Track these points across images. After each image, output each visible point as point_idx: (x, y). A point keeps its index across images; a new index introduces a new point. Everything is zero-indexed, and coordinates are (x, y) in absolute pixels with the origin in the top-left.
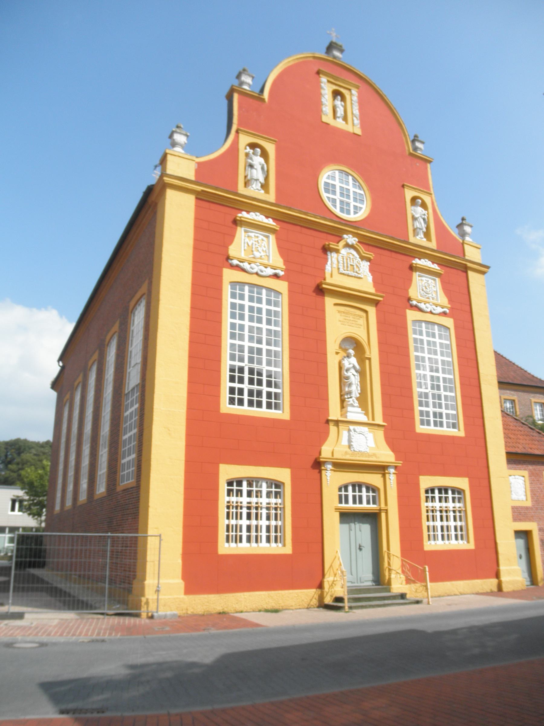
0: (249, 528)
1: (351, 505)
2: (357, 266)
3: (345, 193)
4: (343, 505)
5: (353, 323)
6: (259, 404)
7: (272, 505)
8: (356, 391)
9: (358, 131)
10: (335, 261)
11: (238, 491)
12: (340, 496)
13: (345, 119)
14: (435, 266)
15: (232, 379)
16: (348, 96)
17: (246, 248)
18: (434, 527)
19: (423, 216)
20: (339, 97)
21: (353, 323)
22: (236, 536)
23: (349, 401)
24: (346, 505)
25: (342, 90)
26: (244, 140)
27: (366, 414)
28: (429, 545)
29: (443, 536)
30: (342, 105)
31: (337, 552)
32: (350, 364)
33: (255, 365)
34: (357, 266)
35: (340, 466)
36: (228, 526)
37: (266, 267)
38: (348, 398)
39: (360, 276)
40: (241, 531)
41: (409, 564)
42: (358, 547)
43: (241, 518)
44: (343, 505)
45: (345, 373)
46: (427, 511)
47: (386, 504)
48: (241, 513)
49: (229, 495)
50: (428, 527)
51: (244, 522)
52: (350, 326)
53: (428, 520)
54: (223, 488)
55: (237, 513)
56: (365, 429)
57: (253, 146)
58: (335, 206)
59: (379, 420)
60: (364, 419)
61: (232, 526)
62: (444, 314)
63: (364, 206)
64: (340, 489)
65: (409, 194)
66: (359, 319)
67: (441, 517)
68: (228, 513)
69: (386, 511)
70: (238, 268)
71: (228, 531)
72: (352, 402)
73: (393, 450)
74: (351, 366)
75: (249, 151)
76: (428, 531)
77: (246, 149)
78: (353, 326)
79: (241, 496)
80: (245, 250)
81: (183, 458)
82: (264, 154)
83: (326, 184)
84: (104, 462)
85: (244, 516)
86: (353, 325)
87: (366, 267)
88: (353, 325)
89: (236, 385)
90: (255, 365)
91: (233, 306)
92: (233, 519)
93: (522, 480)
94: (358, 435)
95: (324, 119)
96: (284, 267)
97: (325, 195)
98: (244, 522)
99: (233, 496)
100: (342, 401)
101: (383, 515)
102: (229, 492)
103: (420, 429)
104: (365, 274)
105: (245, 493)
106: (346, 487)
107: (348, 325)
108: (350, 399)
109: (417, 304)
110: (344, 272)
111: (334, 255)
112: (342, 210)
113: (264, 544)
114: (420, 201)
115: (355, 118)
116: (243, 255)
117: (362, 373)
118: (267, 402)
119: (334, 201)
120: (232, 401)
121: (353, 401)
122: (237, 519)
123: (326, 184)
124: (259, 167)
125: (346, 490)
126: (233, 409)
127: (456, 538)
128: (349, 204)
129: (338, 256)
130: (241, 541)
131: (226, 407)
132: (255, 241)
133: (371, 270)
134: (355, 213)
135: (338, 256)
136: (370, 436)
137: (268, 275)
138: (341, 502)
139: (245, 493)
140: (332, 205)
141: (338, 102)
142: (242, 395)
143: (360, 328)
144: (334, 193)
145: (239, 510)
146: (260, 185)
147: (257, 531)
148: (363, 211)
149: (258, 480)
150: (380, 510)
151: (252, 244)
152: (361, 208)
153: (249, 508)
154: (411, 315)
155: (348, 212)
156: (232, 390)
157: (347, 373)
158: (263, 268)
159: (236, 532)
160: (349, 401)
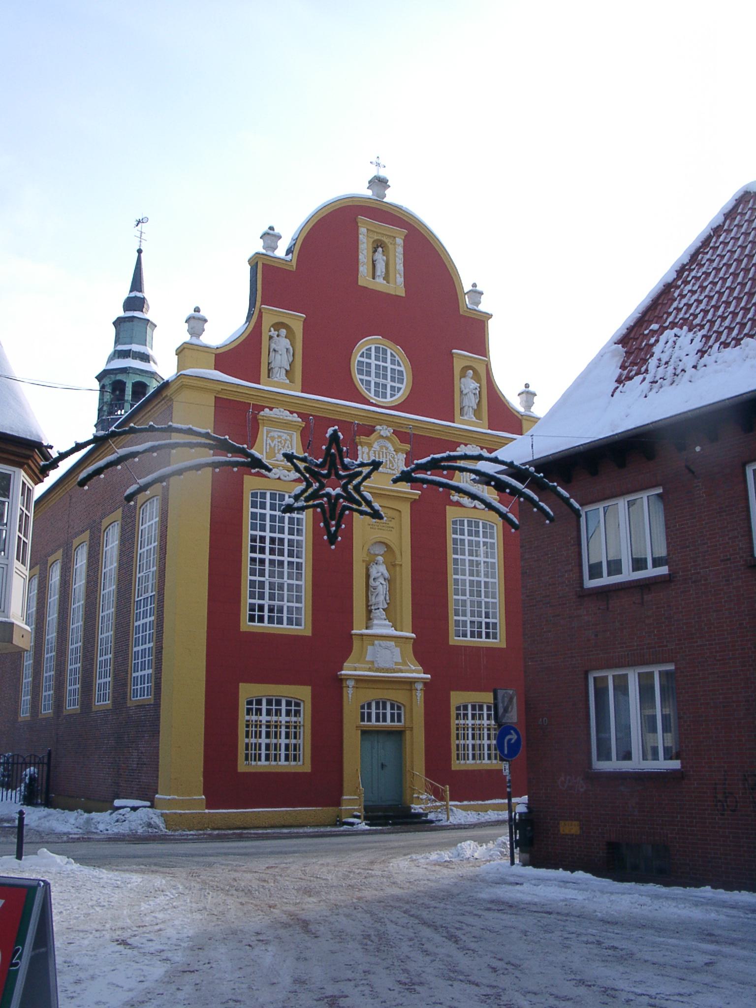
0: (268, 747)
3: (381, 372)
5: (383, 526)
6: (261, 619)
7: (272, 723)
8: (384, 601)
9: (402, 292)
11: (257, 710)
12: (363, 714)
14: (485, 452)
17: (268, 450)
18: (464, 745)
19: (474, 391)
21: (383, 526)
22: (255, 754)
23: (376, 613)
24: (384, 723)
25: (384, 239)
28: (457, 765)
29: (474, 755)
30: (383, 260)
31: (357, 770)
32: (378, 572)
33: (276, 579)
36: (247, 745)
38: (376, 609)
40: (260, 749)
41: (431, 783)
42: (380, 765)
43: (260, 737)
45: (373, 582)
46: (457, 729)
47: (412, 720)
48: (260, 732)
49: (248, 714)
50: (458, 746)
51: (264, 741)
52: (381, 529)
53: (458, 738)
54: (243, 707)
55: (256, 732)
57: (278, 326)
58: (369, 390)
61: (252, 744)
63: (403, 386)
66: (391, 521)
67: (473, 735)
68: (247, 732)
69: (411, 729)
71: (247, 749)
74: (380, 574)
75: (273, 334)
76: (458, 750)
77: (270, 331)
78: (383, 530)
79: (261, 715)
80: (266, 452)
82: (290, 335)
83: (401, 381)
85: (264, 734)
86: (384, 528)
87: (402, 460)
88: (384, 528)
90: (276, 579)
91: (254, 516)
92: (252, 737)
93: (406, 690)
94: (383, 650)
95: (361, 283)
97: (357, 377)
98: (264, 741)
99: (252, 715)
100: (369, 612)
101: (408, 733)
102: (249, 712)
105: (264, 712)
107: (378, 529)
108: (377, 611)
109: (459, 498)
112: (377, 394)
114: (471, 371)
117: (390, 581)
118: (269, 617)
119: (368, 383)
120: (252, 619)
122: (256, 737)
123: (401, 381)
126: (273, 628)
127: (489, 758)
128: (386, 385)
129: (369, 450)
130: (260, 760)
131: (247, 625)
132: (278, 442)
134: (392, 396)
135: (369, 450)
136: (397, 651)
137: (292, 479)
138: (363, 720)
139: (264, 712)
140: (366, 389)
141: (379, 256)
142: (263, 611)
143: (391, 531)
144: (368, 374)
145: (259, 729)
146: (284, 372)
147: (295, 750)
148: (402, 392)
150: (405, 727)
151: (275, 445)
152: (399, 389)
153: (287, 727)
155: (384, 396)
157: (375, 582)
159: (255, 750)
160: (376, 613)
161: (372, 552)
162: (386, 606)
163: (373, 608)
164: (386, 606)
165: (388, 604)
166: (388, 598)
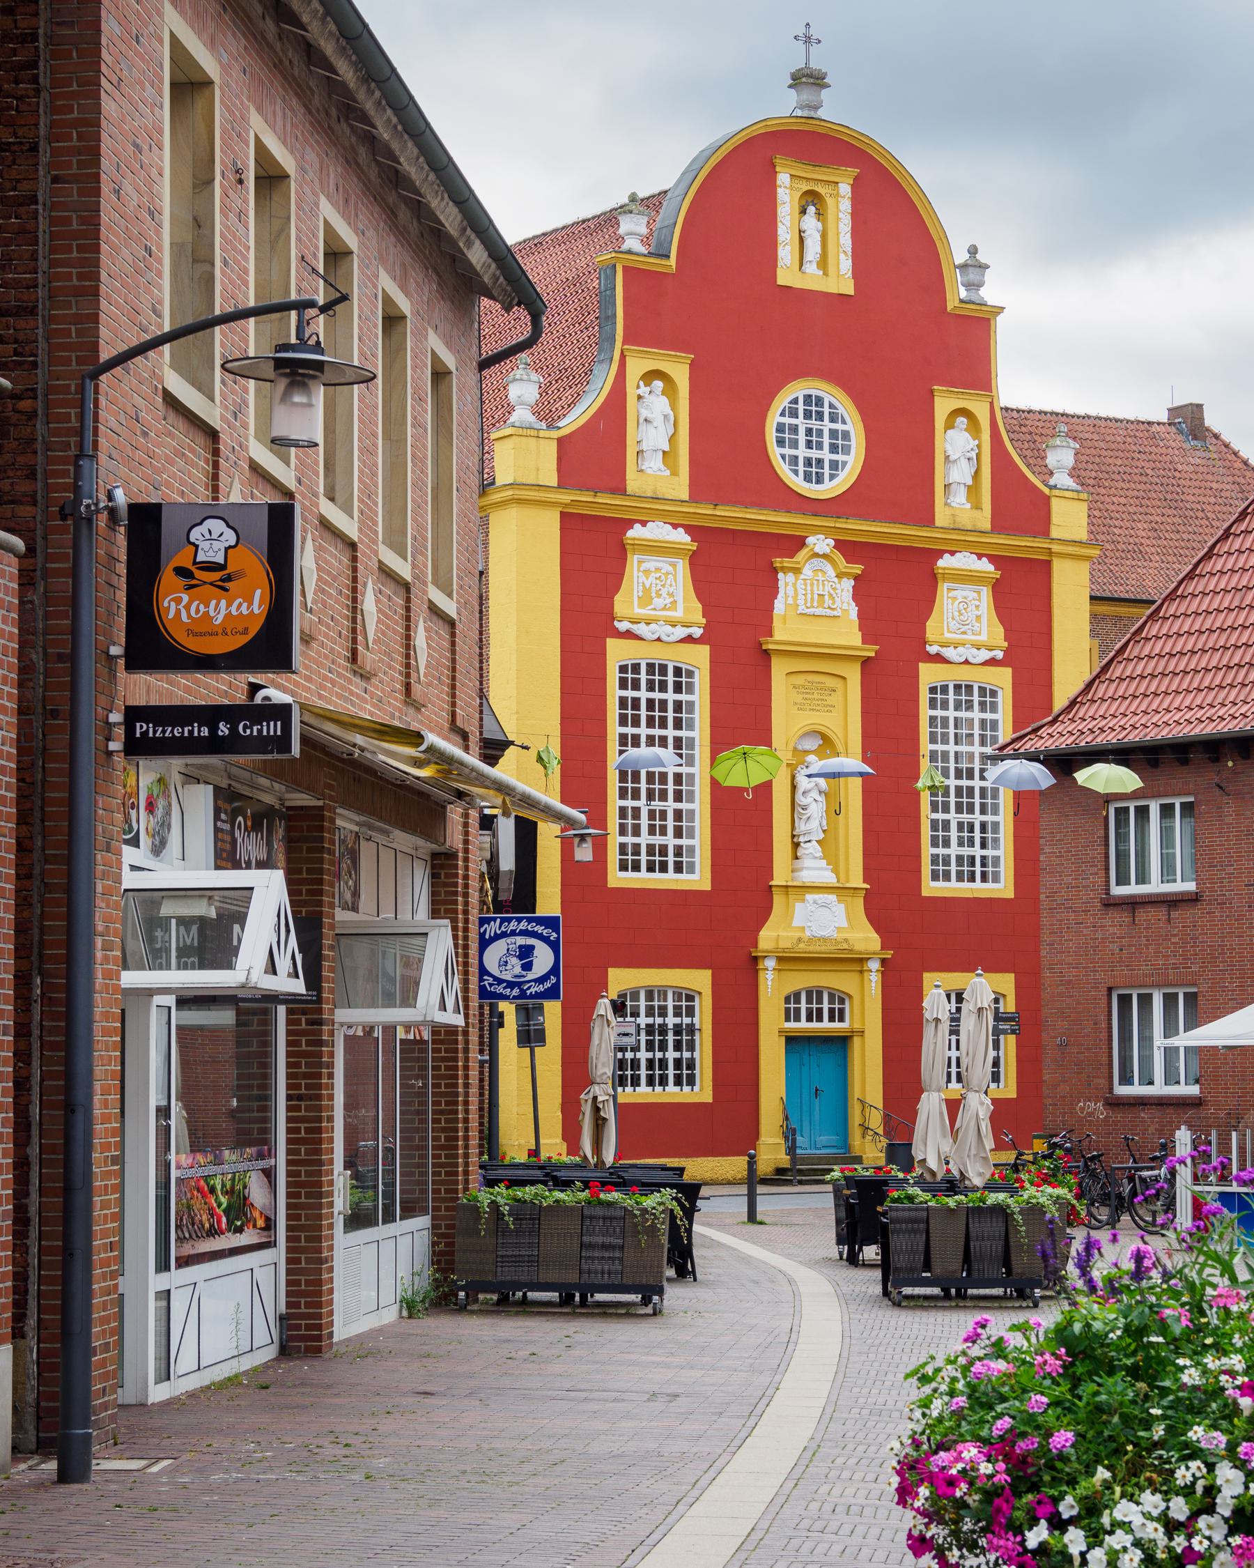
1: (803, 1024)
2: (831, 595)
4: (792, 1025)
10: (790, 590)
12: (787, 1010)
13: (823, 263)
15: (623, 684)
16: (830, 201)
20: (811, 210)
25: (820, 189)
26: (637, 366)
27: (836, 871)
34: (831, 595)
35: (787, 960)
37: (674, 626)
39: (835, 613)
44: (792, 1025)
45: (802, 799)
47: (863, 1024)
56: (832, 898)
59: (857, 881)
60: (829, 878)
62: (992, 662)
64: (787, 1000)
65: (943, 405)
70: (629, 635)
72: (811, 850)
73: (878, 931)
77: (638, 387)
81: (560, 1083)
84: (469, 244)
89: (630, 694)
96: (704, 621)
97: (775, 452)
103: (931, 888)
104: (845, 606)
106: (797, 996)
110: (806, 611)
111: (790, 577)
113: (671, 1088)
115: (842, 256)
116: (639, 611)
121: (811, 849)
124: (659, 421)
125: (798, 1001)
133: (856, 597)
136: (840, 909)
138: (787, 1019)
149: (655, 200)
154: (928, 675)
156: (623, 702)
158: (669, 629)
161: (800, 747)
162: (822, 836)
163: (802, 839)
164: (822, 836)
165: (824, 831)
166: (824, 823)
